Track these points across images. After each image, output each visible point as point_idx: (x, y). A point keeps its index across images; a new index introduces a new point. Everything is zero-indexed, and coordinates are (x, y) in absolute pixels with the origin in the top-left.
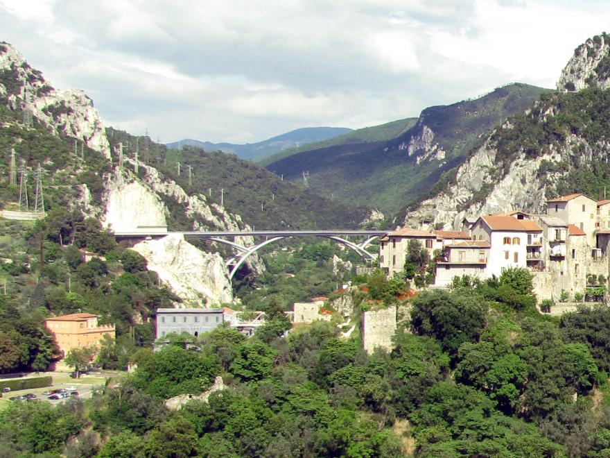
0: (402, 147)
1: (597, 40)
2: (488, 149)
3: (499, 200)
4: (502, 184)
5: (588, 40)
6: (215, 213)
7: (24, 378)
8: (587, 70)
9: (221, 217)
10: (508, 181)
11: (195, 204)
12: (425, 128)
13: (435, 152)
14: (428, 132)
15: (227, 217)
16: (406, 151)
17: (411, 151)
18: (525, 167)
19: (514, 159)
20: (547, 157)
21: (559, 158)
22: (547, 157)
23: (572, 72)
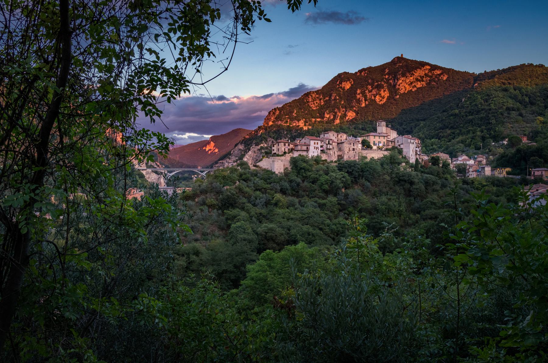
0: (204, 148)
1: (275, 109)
2: (241, 144)
3: (247, 159)
4: (248, 154)
5: (273, 109)
6: (157, 165)
7: (180, 136)
8: (272, 118)
9: (158, 166)
10: (250, 153)
11: (221, 102)
12: (211, 142)
13: (215, 150)
14: (212, 144)
15: (160, 166)
16: (205, 150)
17: (207, 149)
18: (254, 148)
19: (252, 146)
20: (262, 145)
21: (266, 145)
22: (262, 145)
23: (268, 119)
